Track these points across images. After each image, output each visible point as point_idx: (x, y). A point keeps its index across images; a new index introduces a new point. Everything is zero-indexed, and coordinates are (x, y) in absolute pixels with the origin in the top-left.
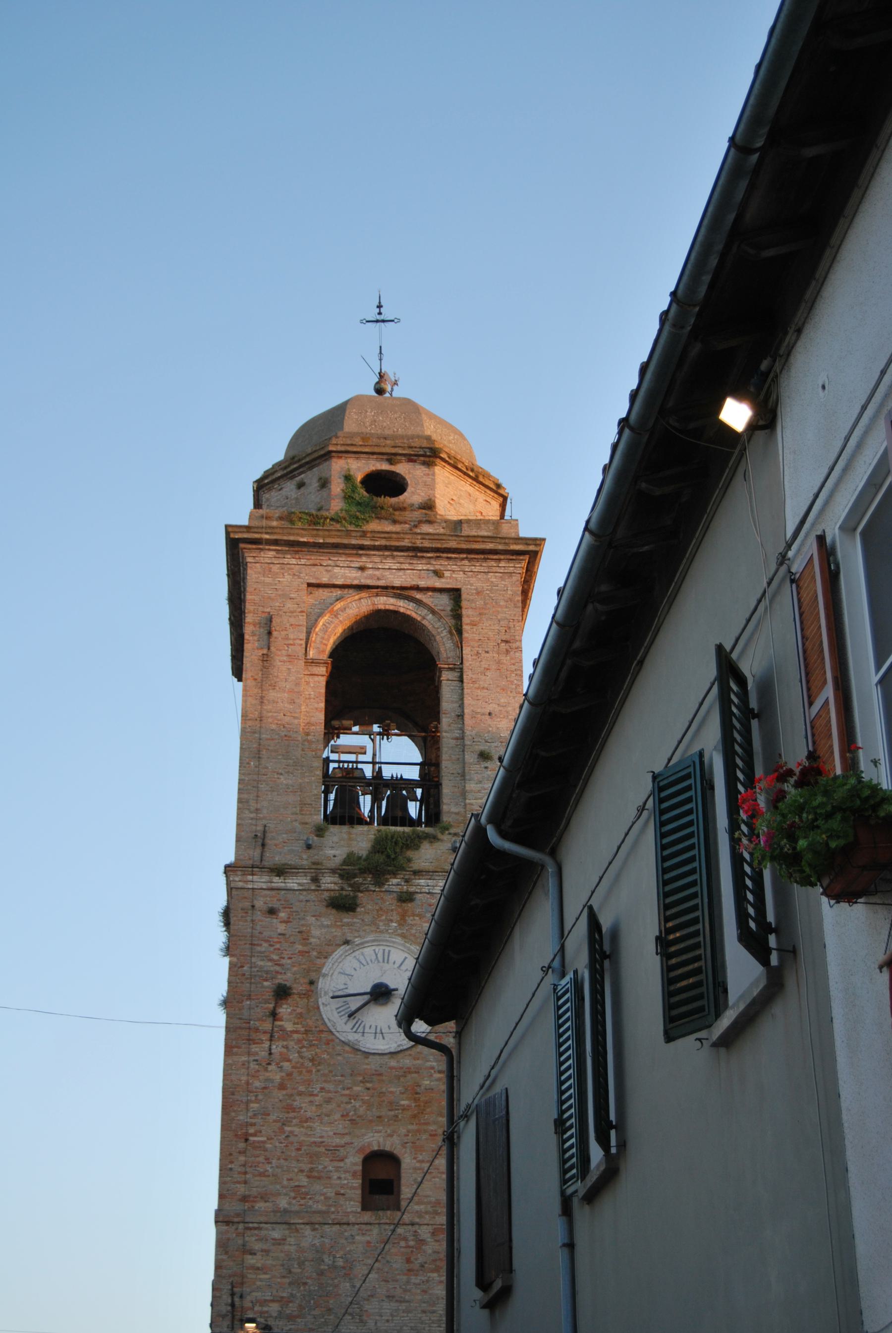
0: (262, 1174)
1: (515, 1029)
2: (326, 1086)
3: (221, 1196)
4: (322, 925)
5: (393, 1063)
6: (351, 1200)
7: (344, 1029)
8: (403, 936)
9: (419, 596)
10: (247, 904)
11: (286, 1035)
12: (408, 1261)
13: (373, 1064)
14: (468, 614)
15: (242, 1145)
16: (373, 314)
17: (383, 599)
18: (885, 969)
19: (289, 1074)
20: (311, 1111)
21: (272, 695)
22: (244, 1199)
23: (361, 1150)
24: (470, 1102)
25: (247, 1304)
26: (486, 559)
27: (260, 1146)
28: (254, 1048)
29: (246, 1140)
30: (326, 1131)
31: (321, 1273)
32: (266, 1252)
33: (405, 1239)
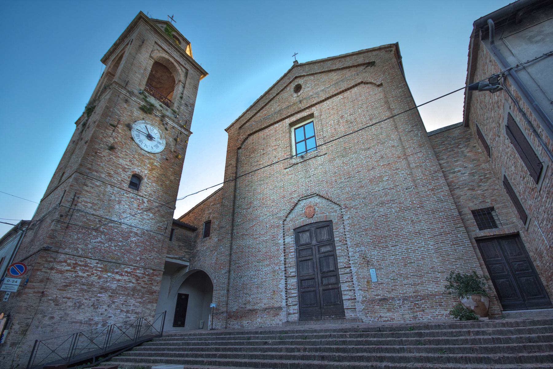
0: (99, 165)
4: (137, 113)
11: (118, 132)
12: (138, 206)
13: (143, 152)
15: (94, 154)
19: (116, 143)
22: (89, 169)
23: (133, 172)
27: (101, 157)
28: (107, 130)
29: (96, 153)
31: (110, 200)
32: (93, 188)
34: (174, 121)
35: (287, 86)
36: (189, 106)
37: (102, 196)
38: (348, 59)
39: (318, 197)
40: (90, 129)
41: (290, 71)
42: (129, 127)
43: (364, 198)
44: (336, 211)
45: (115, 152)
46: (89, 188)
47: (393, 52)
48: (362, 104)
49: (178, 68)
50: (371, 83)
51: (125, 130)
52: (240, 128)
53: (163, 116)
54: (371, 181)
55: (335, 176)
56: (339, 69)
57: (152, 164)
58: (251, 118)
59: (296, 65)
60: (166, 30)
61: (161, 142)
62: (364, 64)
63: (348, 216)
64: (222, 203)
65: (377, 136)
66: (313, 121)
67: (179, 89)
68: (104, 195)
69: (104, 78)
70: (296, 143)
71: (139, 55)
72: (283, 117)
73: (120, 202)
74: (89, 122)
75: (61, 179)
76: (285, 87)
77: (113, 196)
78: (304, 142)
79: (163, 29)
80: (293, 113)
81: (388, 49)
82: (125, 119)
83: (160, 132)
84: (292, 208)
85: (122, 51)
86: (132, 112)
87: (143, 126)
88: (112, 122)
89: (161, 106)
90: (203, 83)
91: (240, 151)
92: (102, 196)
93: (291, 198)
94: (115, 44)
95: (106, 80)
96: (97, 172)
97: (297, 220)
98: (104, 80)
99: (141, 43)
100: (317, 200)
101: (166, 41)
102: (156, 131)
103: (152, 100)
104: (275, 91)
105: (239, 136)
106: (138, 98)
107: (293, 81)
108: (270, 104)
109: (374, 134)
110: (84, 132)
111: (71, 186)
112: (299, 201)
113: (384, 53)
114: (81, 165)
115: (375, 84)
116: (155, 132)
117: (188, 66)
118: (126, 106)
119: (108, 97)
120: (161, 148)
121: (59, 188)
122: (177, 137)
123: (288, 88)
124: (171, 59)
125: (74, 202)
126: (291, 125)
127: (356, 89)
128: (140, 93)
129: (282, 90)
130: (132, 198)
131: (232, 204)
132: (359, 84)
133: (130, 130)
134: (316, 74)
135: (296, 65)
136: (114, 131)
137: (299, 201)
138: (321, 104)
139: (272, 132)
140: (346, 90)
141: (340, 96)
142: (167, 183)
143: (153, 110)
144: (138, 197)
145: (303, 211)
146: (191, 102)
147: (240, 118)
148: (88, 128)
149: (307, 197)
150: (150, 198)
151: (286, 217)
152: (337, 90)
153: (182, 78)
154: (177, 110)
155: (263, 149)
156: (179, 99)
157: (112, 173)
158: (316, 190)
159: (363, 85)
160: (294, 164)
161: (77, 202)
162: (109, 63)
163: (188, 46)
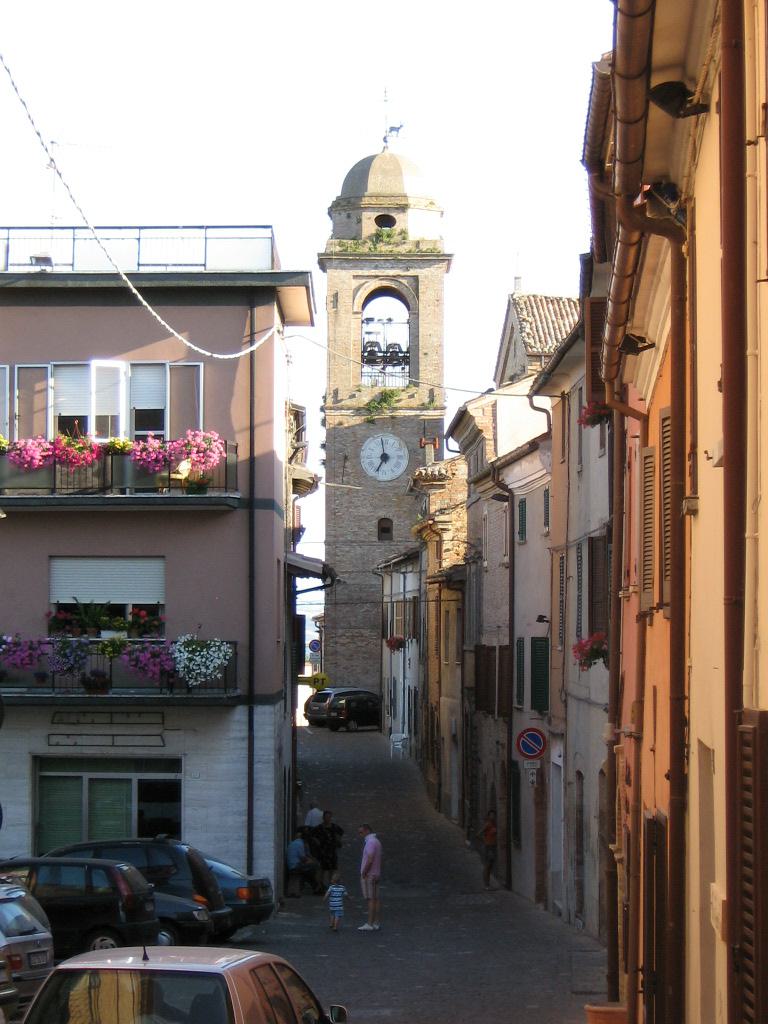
1: (184, 227)
3: (327, 535)
5: (389, 484)
7: (371, 472)
8: (394, 434)
9: (400, 280)
14: (421, 288)
18: (646, 413)
20: (359, 503)
22: (335, 536)
24: (597, 512)
30: (364, 511)
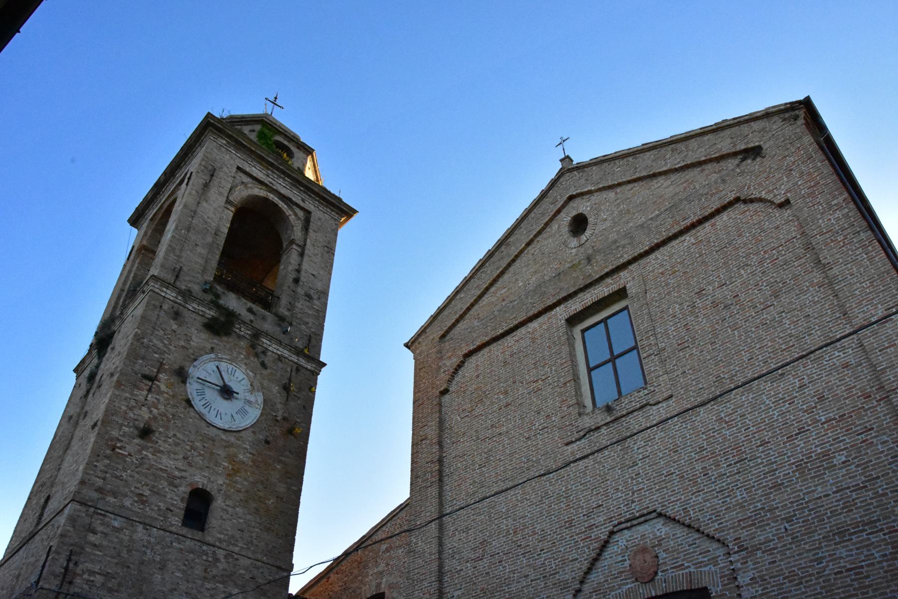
2: (178, 434)
4: (200, 338)
6: (175, 516)
8: (246, 364)
10: (157, 304)
11: (160, 392)
13: (212, 432)
15: (108, 452)
16: (272, 99)
17: (272, 196)
19: (155, 418)
21: (204, 204)
22: (99, 490)
23: (191, 484)
25: (78, 570)
26: (327, 207)
29: (113, 450)
31: (142, 563)
32: (106, 535)
33: (207, 555)
34: (280, 343)
35: (551, 220)
36: (315, 297)
37: (124, 554)
38: (693, 143)
39: (661, 521)
40: (103, 389)
41: (553, 184)
42: (182, 375)
43: (788, 520)
44: (714, 561)
45: (152, 442)
46: (99, 536)
47: (801, 121)
48: (748, 255)
49: (288, 212)
50: (760, 200)
51: (172, 384)
52: (443, 336)
53: (257, 335)
54: (800, 467)
55: (702, 459)
56: (676, 170)
57: (231, 458)
58: (468, 309)
59: (568, 168)
60: (261, 135)
61: (252, 399)
62: (735, 154)
63: (751, 574)
64: (409, 544)
65: (798, 339)
66: (626, 308)
67: (292, 258)
68: (129, 551)
69: (134, 261)
70: (590, 370)
71: (204, 204)
72: (549, 302)
73: (164, 566)
74: (100, 373)
75: (41, 515)
76: (547, 224)
77: (148, 551)
78: (610, 365)
79: (253, 137)
80: (572, 290)
81: (787, 115)
82: (173, 358)
83: (247, 375)
84: (594, 555)
85: (169, 197)
86: (188, 340)
87: (211, 366)
88: (146, 371)
89: (250, 310)
90: (348, 235)
91: (446, 398)
92: (124, 554)
93: (590, 527)
94: (156, 185)
95: (136, 265)
96: (115, 494)
97: (612, 589)
98: (132, 266)
99: (207, 178)
100: (659, 528)
101: (261, 160)
102: (240, 375)
103: (232, 302)
104: (522, 238)
105: (441, 358)
106: (201, 302)
107: (563, 206)
108: (512, 269)
109: (791, 335)
110: (91, 395)
111: (62, 536)
112: (612, 533)
113: (779, 123)
114: (82, 482)
115: (772, 203)
116: (238, 378)
117: (310, 205)
118: (175, 327)
119: (139, 312)
120: (254, 414)
121: (37, 537)
122: (290, 380)
123: (555, 226)
124: (271, 196)
125: (67, 576)
126: (572, 321)
127: (724, 216)
128: (205, 291)
129: (539, 233)
130: (191, 551)
131: (434, 548)
132: (731, 204)
133: (184, 382)
134: (619, 185)
135: (568, 168)
136: (149, 390)
137: (612, 533)
138: (642, 262)
139: (523, 343)
140: (701, 222)
141: (688, 238)
142: (271, 502)
143: (232, 324)
144: (205, 548)
145: (627, 563)
146: (319, 286)
147: (440, 311)
148: (99, 386)
149: (632, 522)
150: (231, 548)
151: (582, 582)
152: (678, 223)
153: (297, 234)
154: (287, 313)
155: (506, 393)
156: (292, 285)
157: (147, 493)
158: (653, 501)
159: (741, 207)
160: (591, 431)
161: (75, 574)
162: (145, 225)
163: (309, 158)
